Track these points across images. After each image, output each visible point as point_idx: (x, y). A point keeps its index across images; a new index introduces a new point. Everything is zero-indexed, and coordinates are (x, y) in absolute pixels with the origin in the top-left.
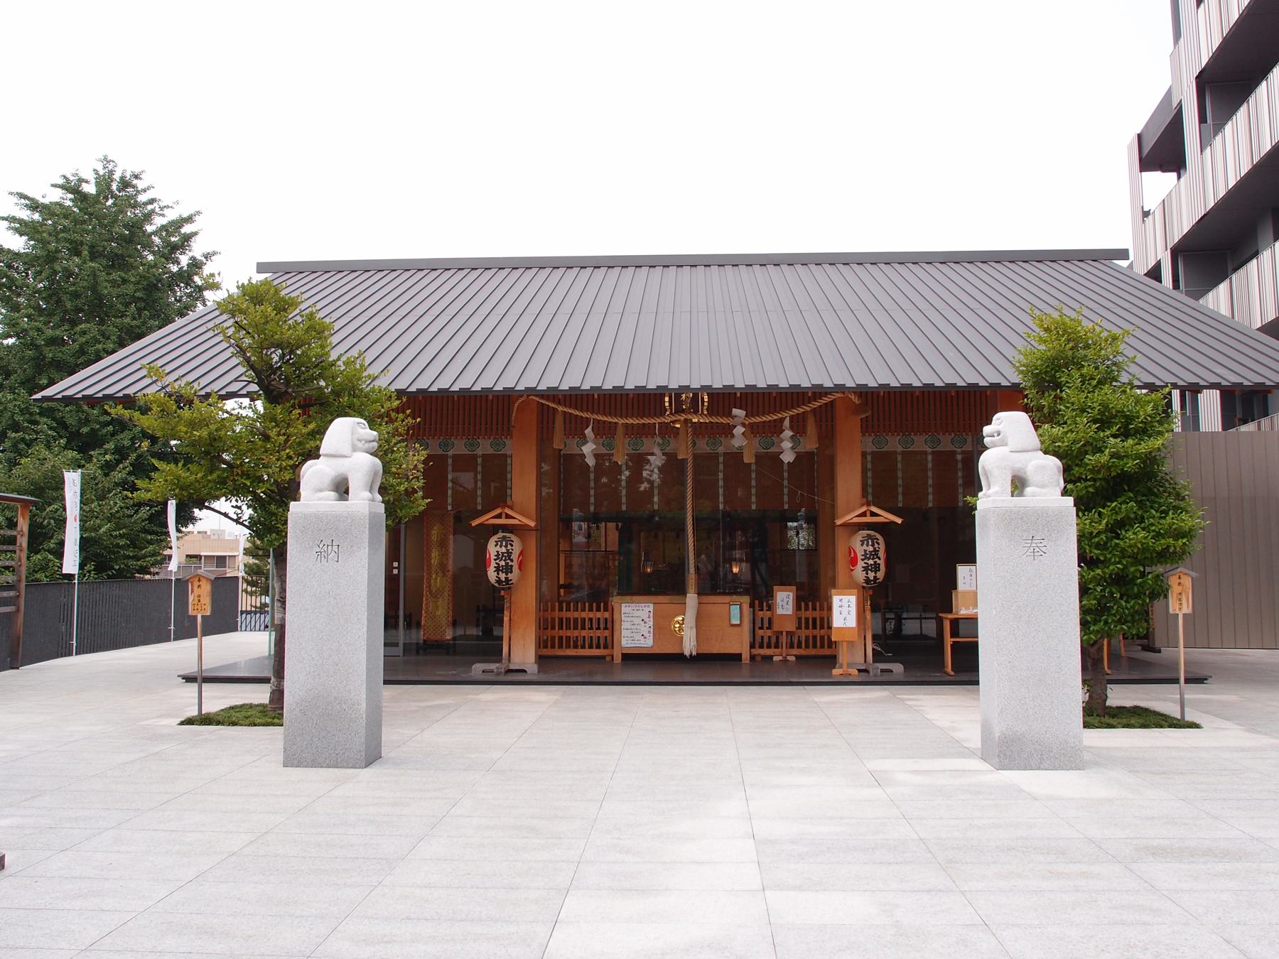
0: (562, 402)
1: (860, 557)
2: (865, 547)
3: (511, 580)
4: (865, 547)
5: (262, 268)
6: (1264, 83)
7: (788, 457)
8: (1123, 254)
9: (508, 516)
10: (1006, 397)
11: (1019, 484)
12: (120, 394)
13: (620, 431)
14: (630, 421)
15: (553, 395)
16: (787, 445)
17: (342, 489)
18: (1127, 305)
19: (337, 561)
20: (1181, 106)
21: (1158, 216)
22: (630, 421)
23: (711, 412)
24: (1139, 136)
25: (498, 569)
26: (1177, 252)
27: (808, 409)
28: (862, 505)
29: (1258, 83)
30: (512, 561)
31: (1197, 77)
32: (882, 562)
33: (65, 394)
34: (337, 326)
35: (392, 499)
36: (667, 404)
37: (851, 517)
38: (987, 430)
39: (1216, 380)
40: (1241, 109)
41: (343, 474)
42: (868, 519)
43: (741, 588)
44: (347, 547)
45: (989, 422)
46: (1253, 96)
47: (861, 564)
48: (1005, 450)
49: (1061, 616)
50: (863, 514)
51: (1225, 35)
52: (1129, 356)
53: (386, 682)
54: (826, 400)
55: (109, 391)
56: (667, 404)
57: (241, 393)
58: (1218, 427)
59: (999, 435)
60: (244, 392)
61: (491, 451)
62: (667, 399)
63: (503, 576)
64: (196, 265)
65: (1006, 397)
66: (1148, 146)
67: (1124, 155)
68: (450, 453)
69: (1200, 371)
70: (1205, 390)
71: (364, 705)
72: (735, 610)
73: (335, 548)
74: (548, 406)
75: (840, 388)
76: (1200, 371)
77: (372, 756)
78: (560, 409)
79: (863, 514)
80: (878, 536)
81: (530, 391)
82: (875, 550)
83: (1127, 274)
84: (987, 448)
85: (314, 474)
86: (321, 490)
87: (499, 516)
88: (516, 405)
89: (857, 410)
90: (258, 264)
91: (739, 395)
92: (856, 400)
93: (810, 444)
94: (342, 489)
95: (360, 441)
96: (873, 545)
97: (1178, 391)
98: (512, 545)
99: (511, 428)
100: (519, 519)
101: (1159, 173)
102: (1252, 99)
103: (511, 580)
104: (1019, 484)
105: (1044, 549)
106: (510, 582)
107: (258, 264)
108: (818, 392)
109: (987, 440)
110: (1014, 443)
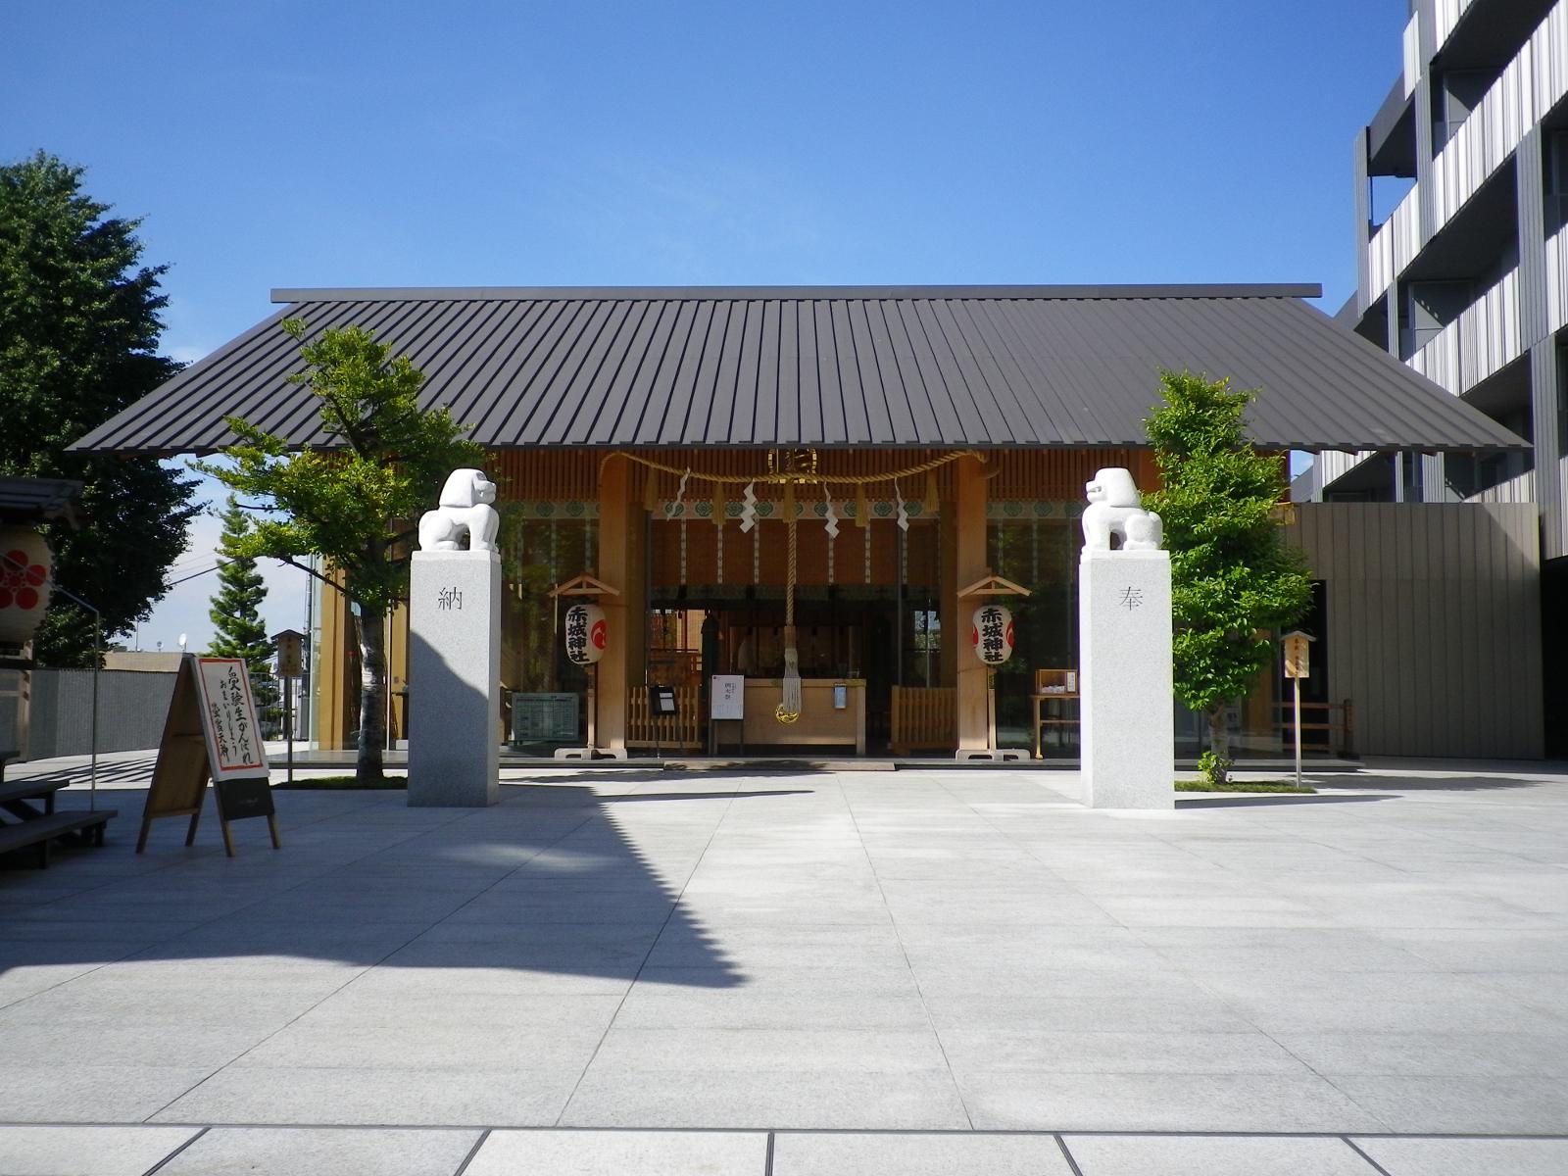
0: (644, 454)
1: (981, 632)
2: (986, 623)
3: (585, 654)
4: (986, 623)
6: (1499, 80)
7: (903, 524)
8: (1315, 291)
9: (590, 586)
11: (1116, 541)
13: (719, 490)
14: (731, 480)
16: (904, 515)
17: (463, 540)
20: (1414, 98)
22: (731, 480)
23: (820, 471)
25: (987, 645)
27: (929, 468)
28: (988, 575)
29: (1494, 80)
30: (1001, 635)
31: (1431, 64)
34: (428, 372)
36: (770, 463)
37: (974, 589)
38: (1090, 486)
39: (1441, 441)
40: (1476, 108)
41: (462, 525)
45: (1092, 478)
46: (1488, 94)
47: (981, 639)
49: (1155, 662)
50: (988, 586)
51: (1462, 14)
52: (850, 440)
54: (948, 458)
56: (770, 463)
57: (188, 447)
59: (1100, 490)
60: (191, 446)
61: (567, 516)
62: (770, 457)
63: (576, 649)
64: (148, 279)
69: (1471, 430)
70: (1323, 452)
72: (840, 693)
73: (458, 596)
74: (640, 463)
76: (1471, 430)
78: (653, 466)
81: (629, 447)
82: (996, 626)
83: (1318, 317)
84: (1089, 504)
85: (432, 526)
86: (442, 540)
87: (579, 586)
88: (603, 462)
89: (983, 469)
90: (274, 291)
91: (851, 452)
92: (982, 459)
93: (929, 509)
94: (463, 540)
96: (994, 620)
97: (1443, 453)
98: (999, 619)
99: (598, 488)
100: (601, 588)
101: (1393, 178)
102: (1486, 98)
103: (585, 654)
104: (1116, 541)
105: (1140, 599)
106: (585, 657)
107: (274, 291)
109: (1090, 496)
110: (1113, 499)
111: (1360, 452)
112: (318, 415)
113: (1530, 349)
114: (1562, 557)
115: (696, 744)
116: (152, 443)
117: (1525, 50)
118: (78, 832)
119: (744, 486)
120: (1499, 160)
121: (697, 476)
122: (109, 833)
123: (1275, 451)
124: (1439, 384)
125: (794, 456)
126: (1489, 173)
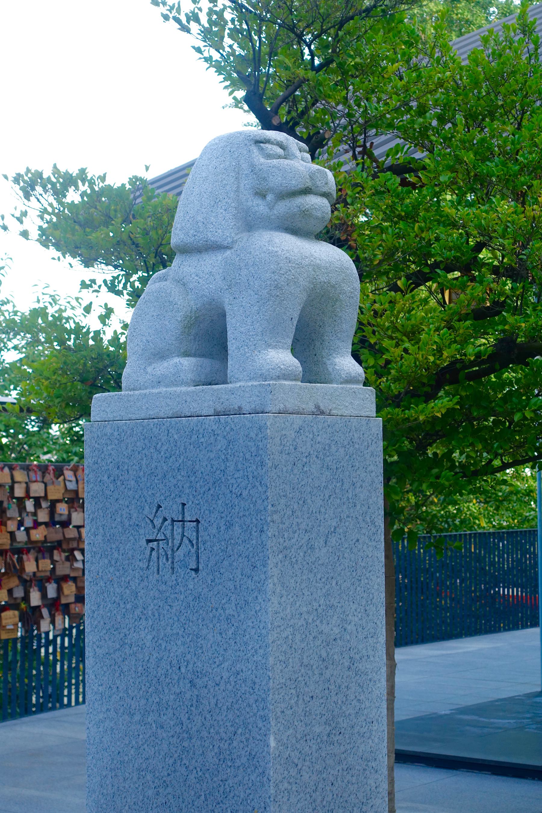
19: (196, 570)
44: (218, 528)
95: (262, 195)
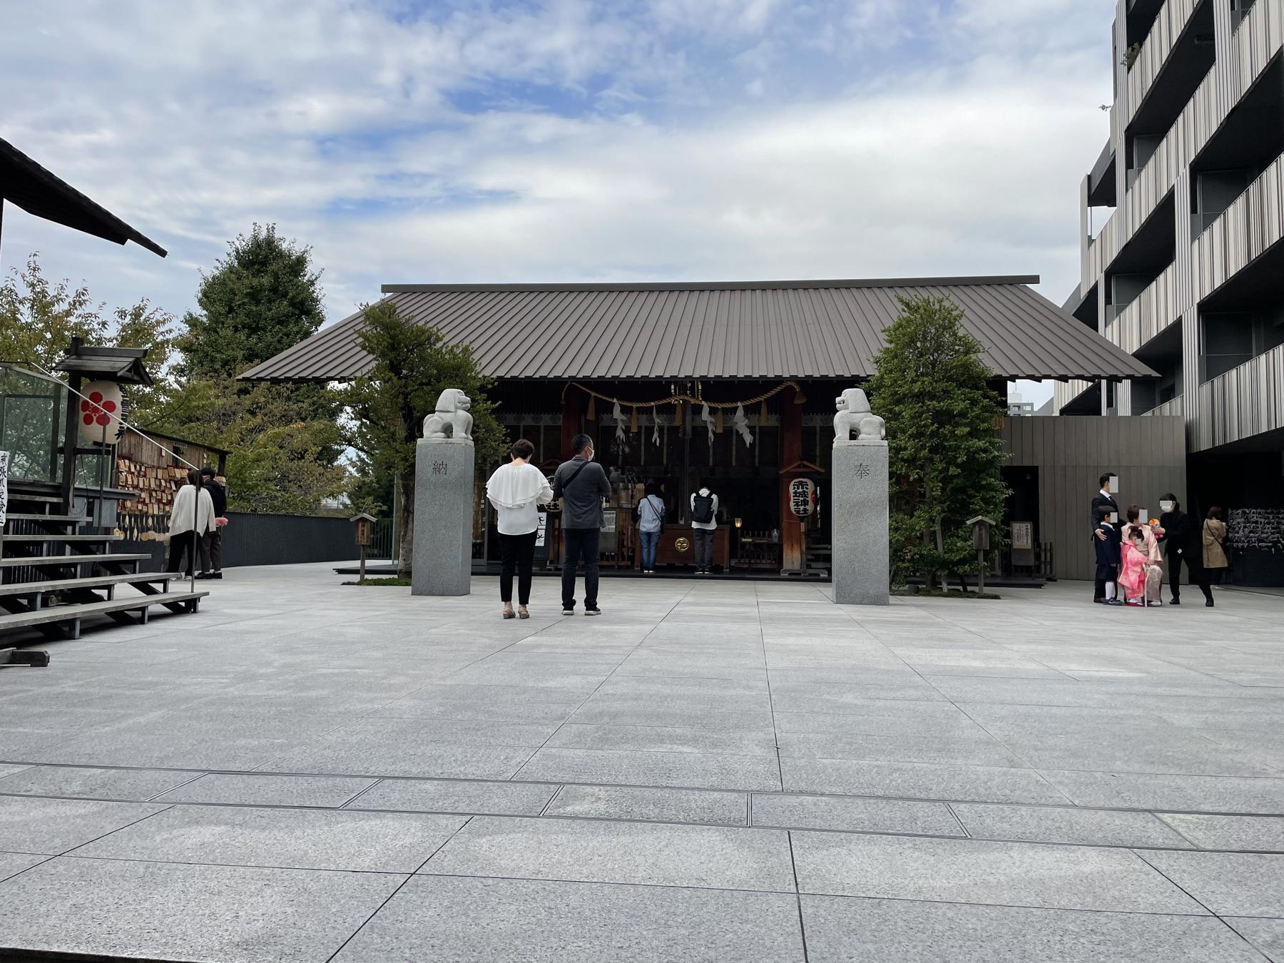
5: (385, 289)
10: (853, 382)
11: (853, 435)
12: (297, 377)
15: (587, 381)
17: (448, 430)
18: (988, 319)
21: (1098, 242)
24: (1089, 177)
26: (1109, 274)
32: (809, 499)
33: (272, 375)
35: (406, 955)
38: (838, 399)
42: (804, 470)
43: (623, 449)
48: (847, 411)
53: (473, 574)
55: (303, 374)
58: (1129, 413)
61: (550, 423)
65: (853, 382)
66: (1096, 183)
67: (1077, 193)
68: (522, 425)
71: (460, 558)
75: (794, 378)
77: (468, 593)
78: (593, 394)
79: (799, 466)
80: (804, 480)
85: (431, 424)
90: (383, 286)
94: (448, 430)
96: (802, 488)
104: (853, 435)
107: (383, 286)
108: (778, 380)
111: (1070, 381)
112: (483, 366)
113: (1181, 317)
114: (1200, 452)
115: (102, 546)
116: (301, 375)
117: (1180, 119)
118: (183, 604)
119: (735, 409)
120: (1165, 192)
121: (748, 403)
122: (200, 606)
123: (999, 384)
124: (1116, 343)
125: (685, 384)
126: (1158, 201)
